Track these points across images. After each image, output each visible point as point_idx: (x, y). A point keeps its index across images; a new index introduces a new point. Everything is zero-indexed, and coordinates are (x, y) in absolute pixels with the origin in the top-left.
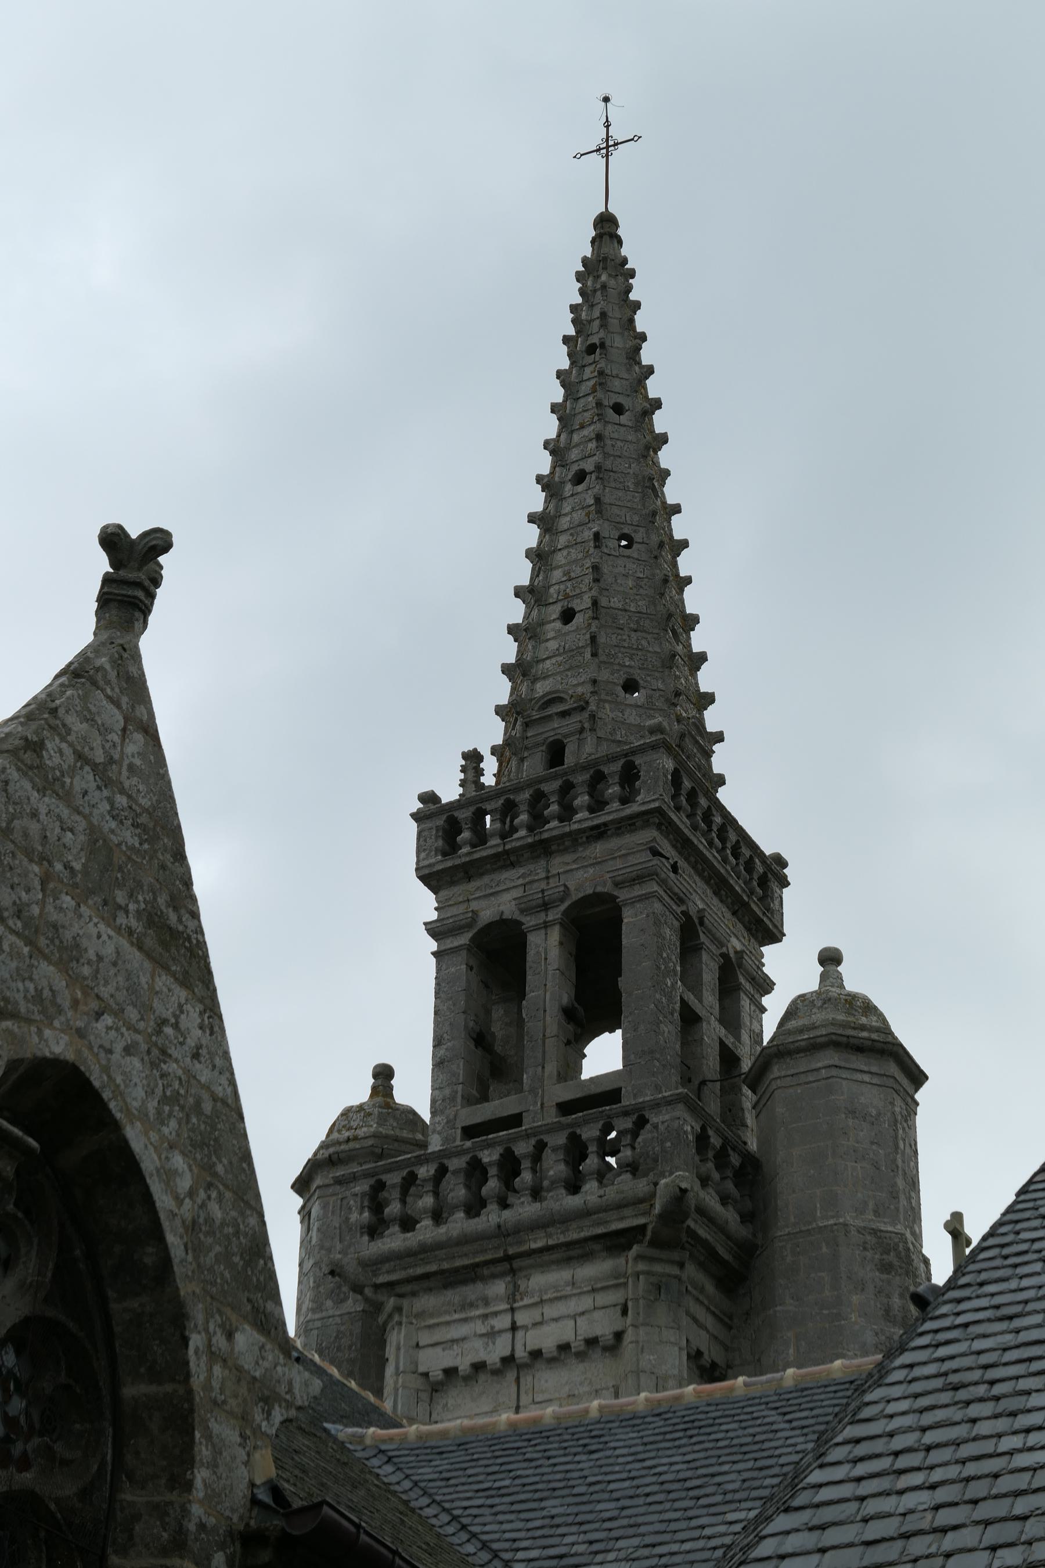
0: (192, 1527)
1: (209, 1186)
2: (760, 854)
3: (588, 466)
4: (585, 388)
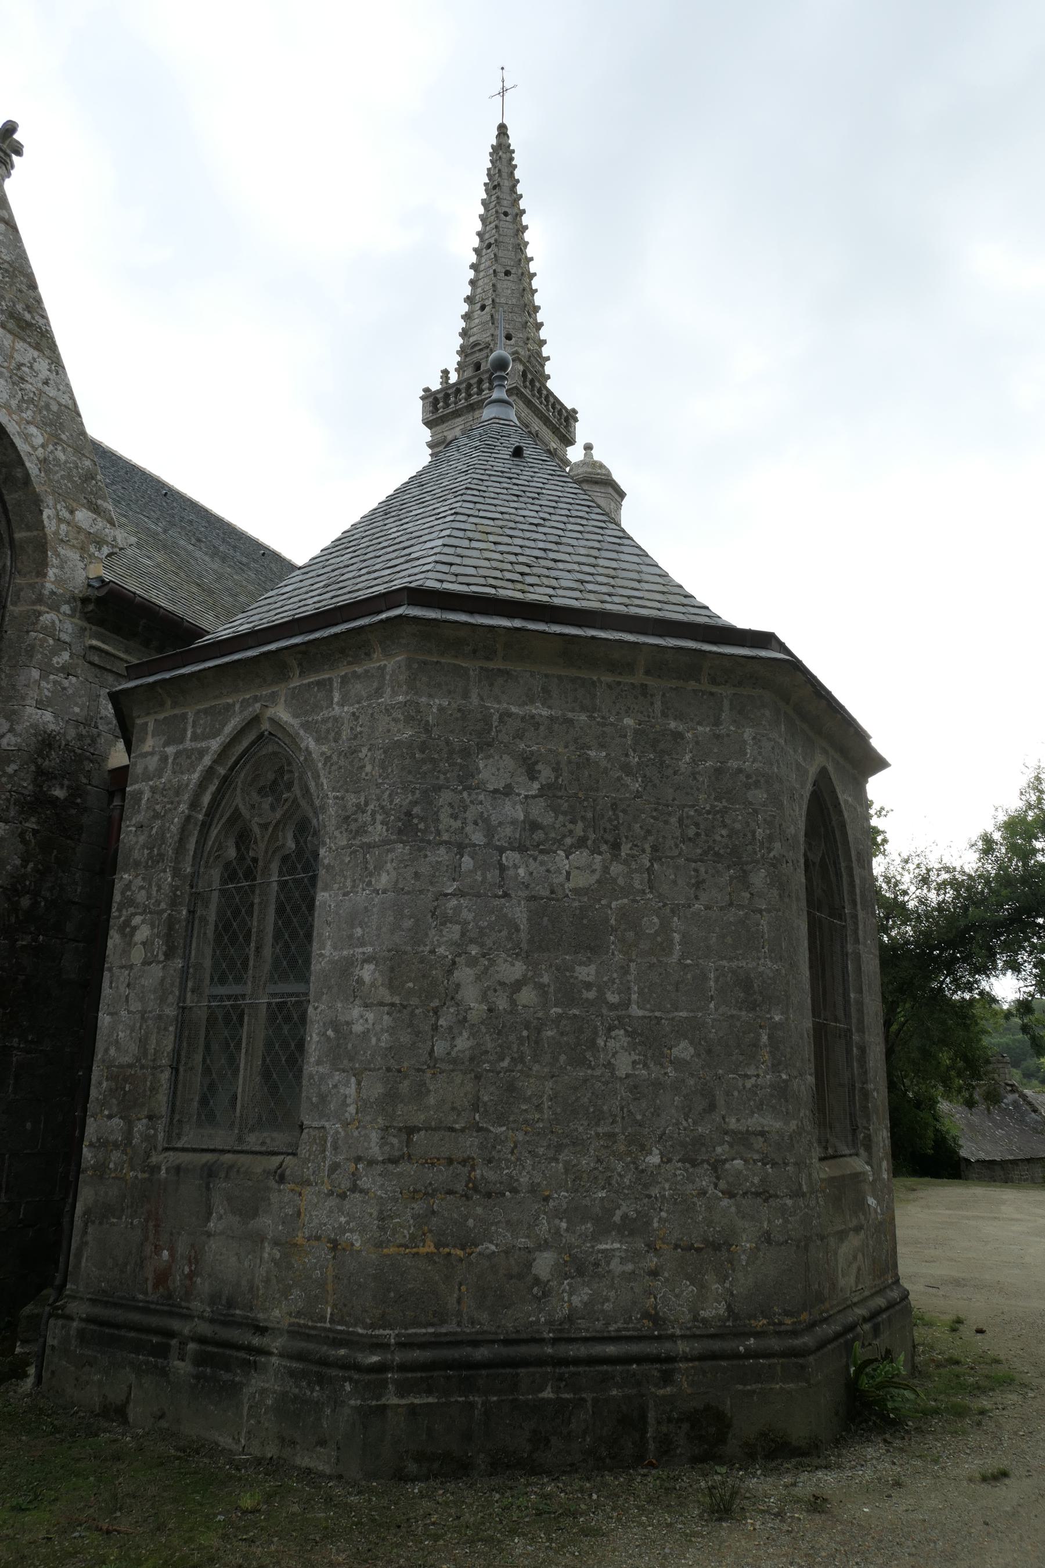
0: (46, 592)
1: (56, 444)
2: (565, 408)
3: (492, 241)
4: (492, 205)
